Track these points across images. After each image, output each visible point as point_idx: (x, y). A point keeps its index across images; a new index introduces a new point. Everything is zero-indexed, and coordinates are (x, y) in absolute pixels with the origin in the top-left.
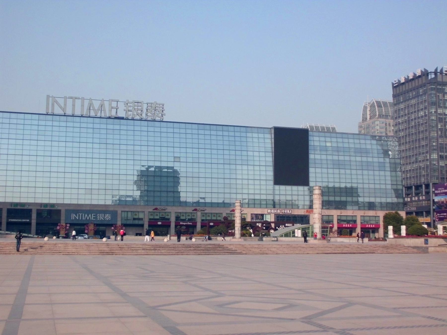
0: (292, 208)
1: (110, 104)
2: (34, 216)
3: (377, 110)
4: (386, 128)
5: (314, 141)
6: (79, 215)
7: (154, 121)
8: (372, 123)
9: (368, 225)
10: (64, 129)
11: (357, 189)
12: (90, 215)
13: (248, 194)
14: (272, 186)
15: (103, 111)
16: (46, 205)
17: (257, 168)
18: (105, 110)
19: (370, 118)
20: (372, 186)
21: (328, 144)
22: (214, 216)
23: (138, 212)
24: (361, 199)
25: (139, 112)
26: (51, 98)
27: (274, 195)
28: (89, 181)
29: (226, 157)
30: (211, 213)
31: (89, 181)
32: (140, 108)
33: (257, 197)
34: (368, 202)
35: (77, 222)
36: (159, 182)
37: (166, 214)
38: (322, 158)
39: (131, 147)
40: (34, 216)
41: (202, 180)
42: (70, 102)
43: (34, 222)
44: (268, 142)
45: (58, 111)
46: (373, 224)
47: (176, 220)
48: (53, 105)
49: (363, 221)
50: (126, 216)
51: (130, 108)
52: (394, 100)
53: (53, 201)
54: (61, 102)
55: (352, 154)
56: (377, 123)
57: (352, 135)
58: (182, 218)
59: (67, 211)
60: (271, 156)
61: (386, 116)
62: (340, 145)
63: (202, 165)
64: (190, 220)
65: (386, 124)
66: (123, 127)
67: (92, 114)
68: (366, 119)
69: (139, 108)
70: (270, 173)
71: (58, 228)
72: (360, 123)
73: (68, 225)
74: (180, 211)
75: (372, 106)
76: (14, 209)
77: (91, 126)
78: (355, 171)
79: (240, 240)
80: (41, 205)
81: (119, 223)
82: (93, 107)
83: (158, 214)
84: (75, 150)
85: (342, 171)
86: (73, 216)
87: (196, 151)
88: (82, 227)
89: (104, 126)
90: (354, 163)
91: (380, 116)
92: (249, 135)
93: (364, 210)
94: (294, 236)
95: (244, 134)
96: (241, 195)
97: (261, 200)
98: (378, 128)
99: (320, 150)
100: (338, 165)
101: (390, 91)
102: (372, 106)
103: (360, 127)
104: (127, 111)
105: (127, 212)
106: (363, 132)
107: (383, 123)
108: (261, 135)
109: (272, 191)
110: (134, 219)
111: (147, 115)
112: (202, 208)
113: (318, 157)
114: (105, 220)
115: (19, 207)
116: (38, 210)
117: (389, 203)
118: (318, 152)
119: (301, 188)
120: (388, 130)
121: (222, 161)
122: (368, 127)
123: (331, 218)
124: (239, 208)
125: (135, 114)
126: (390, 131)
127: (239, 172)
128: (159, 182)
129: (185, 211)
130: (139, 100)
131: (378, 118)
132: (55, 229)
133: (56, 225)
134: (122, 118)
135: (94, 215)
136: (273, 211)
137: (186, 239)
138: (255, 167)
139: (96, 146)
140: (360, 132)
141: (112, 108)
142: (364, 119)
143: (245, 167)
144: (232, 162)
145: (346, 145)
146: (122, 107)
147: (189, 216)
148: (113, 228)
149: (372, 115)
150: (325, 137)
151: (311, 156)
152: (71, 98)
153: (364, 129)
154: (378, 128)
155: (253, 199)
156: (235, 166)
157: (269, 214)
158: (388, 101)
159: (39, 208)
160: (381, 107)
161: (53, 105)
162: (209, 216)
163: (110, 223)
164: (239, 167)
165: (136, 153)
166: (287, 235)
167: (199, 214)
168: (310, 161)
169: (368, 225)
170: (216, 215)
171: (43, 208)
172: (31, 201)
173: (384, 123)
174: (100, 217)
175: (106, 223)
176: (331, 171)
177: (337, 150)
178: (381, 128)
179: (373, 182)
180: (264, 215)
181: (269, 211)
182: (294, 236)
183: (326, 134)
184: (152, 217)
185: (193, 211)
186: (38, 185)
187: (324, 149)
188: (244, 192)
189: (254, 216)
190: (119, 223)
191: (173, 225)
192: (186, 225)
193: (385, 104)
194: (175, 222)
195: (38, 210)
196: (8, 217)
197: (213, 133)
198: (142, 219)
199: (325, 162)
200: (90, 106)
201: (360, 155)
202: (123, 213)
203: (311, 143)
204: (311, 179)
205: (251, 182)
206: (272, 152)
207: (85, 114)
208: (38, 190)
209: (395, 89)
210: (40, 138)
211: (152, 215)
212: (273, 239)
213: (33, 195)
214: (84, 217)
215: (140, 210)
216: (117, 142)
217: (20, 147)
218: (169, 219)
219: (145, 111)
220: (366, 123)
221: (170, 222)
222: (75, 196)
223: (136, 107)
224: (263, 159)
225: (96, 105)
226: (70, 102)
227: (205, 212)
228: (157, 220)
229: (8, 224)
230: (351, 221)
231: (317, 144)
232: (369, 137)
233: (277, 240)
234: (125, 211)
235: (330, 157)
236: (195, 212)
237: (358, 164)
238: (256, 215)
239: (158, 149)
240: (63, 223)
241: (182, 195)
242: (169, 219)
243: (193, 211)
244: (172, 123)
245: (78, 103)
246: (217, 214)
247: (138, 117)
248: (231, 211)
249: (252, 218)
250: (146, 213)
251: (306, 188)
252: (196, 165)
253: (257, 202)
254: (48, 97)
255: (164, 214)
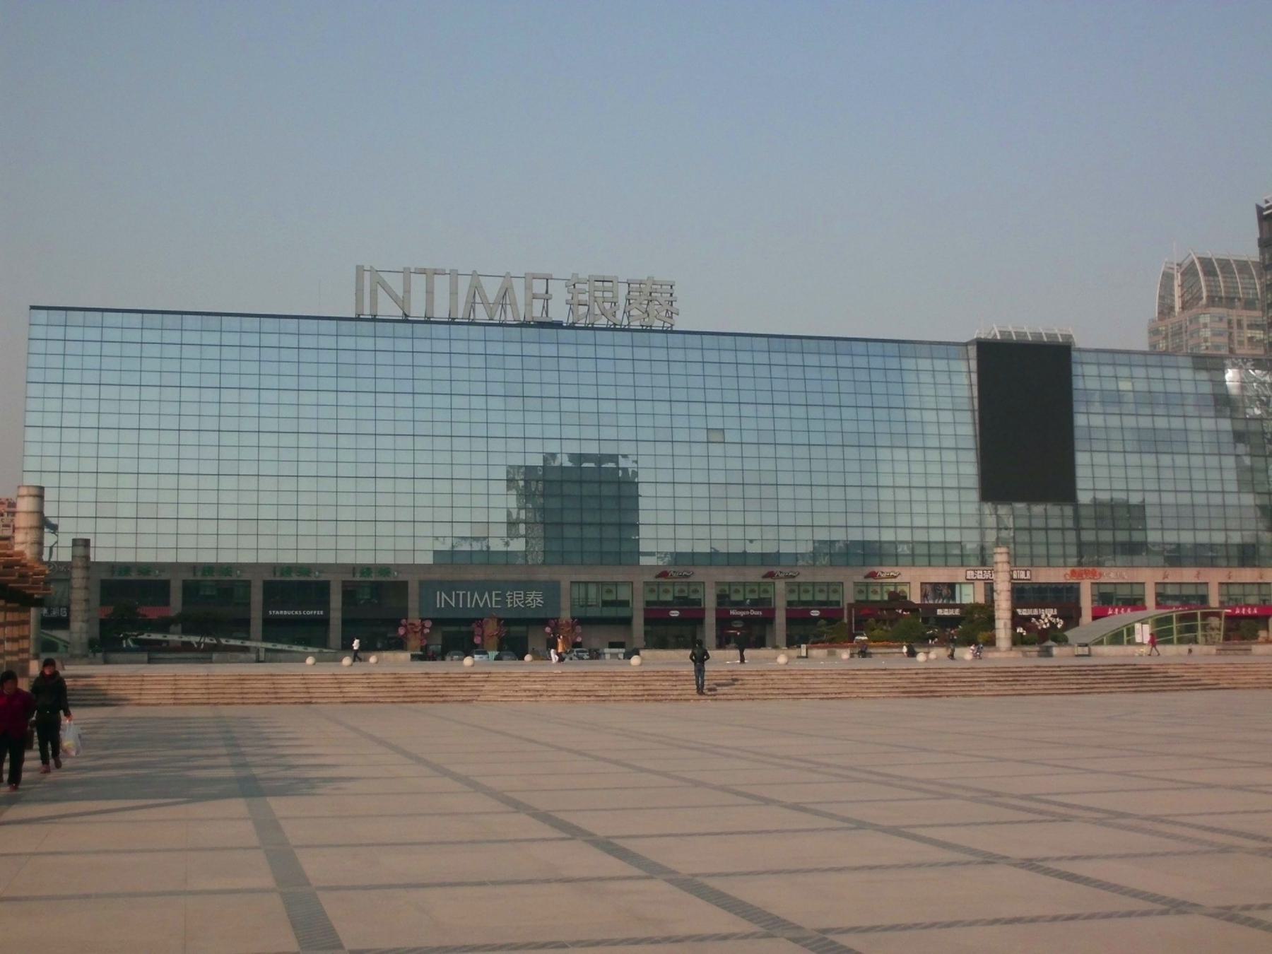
0: (1032, 566)
1: (528, 287)
2: (336, 600)
3: (1203, 284)
4: (1231, 334)
5: (1086, 378)
6: (457, 596)
7: (649, 330)
8: (1191, 322)
9: (1241, 608)
10: (407, 359)
11: (1142, 507)
12: (486, 595)
13: (912, 528)
14: (976, 506)
15: (509, 307)
16: (209, 568)
17: (933, 455)
18: (514, 304)
19: (1183, 308)
20: (1185, 499)
21: (1125, 385)
22: (821, 591)
23: (616, 584)
24: (1153, 537)
25: (607, 305)
26: (367, 275)
27: (1063, 529)
28: (480, 501)
29: (848, 427)
30: (814, 584)
31: (480, 501)
32: (610, 295)
33: (936, 536)
34: (1238, 545)
35: (451, 616)
36: (580, 501)
37: (692, 588)
38: (1109, 424)
39: (589, 406)
40: (336, 600)
41: (785, 492)
42: (419, 282)
43: (336, 616)
44: (962, 381)
45: (388, 308)
46: (1252, 607)
47: (719, 604)
48: (374, 293)
49: (1225, 599)
50: (582, 595)
51: (584, 297)
52: (1262, 253)
53: (385, 559)
54: (396, 283)
55: (1190, 410)
56: (1205, 319)
57: (1142, 357)
58: (736, 597)
59: (422, 584)
60: (970, 420)
61: (1230, 301)
62: (1158, 387)
63: (783, 452)
64: (756, 603)
65: (1229, 322)
66: (567, 351)
67: (481, 314)
68: (1172, 308)
69: (606, 294)
70: (970, 469)
71: (401, 631)
72: (1153, 321)
73: (428, 624)
74: (729, 578)
75: (1189, 272)
76: (301, 582)
77: (478, 347)
78: (1201, 458)
79: (1012, 654)
80: (354, 568)
81: (566, 615)
82: (484, 297)
83: (670, 588)
84: (439, 415)
85: (1166, 460)
86: (441, 599)
87: (766, 411)
88: (463, 629)
89: (514, 348)
90: (1197, 438)
91: (1213, 301)
92: (909, 363)
93: (1228, 566)
94: (1131, 642)
95: (893, 363)
96: (892, 531)
97: (913, 543)
98: (1208, 333)
99: (1103, 402)
100: (1153, 442)
101: (1252, 231)
102: (1189, 272)
103: (1154, 332)
104: (572, 305)
105: (586, 583)
106: (1162, 346)
107: (1221, 319)
108: (940, 365)
109: (977, 518)
110: (605, 603)
111: (627, 312)
112: (787, 571)
113: (1097, 421)
114: (527, 608)
115: (294, 577)
116: (345, 584)
117: (1202, 545)
118: (1097, 407)
119: (1054, 510)
120: (1236, 339)
121: (836, 439)
122: (1178, 332)
123: (1137, 591)
124: (1006, 567)
125: (597, 312)
126: (1241, 343)
127: (885, 467)
128: (580, 501)
129: (741, 579)
130: (607, 274)
131: (1207, 306)
132: (389, 635)
133: (397, 623)
134: (557, 325)
135: (497, 595)
136: (980, 575)
137: (852, 655)
138: (928, 452)
139: (495, 403)
140: (1153, 346)
141: (535, 297)
142: (1166, 310)
143: (900, 454)
144: (867, 440)
145: (1173, 387)
146: (560, 294)
147: (752, 591)
148: (548, 629)
149: (1187, 297)
150: (1162, 367)
151: (1080, 420)
152: (423, 272)
153: (1166, 338)
154: (1208, 333)
155: (825, 542)
156: (872, 450)
157: (970, 582)
158: (1232, 259)
159: (349, 578)
160: (1215, 275)
161: (374, 293)
162: (807, 591)
163: (543, 616)
164: (884, 454)
165: (605, 420)
166: (1116, 639)
167: (780, 585)
168: (1078, 433)
169: (1241, 608)
170: (825, 588)
171: (358, 578)
172: (168, 557)
173: (1225, 320)
174: (515, 600)
175: (530, 615)
176: (1133, 459)
177: (1149, 400)
178: (1214, 335)
179: (1218, 487)
180: (957, 587)
181: (970, 574)
182: (1131, 642)
183: (1149, 357)
184: (653, 598)
185: (765, 577)
186: (346, 514)
187: (1116, 398)
188: (899, 524)
189: (929, 588)
190: (566, 615)
191: (710, 619)
192: (745, 619)
193: (1243, 266)
194: (717, 610)
195: (345, 584)
196: (268, 603)
197: (812, 360)
198: (625, 604)
199: (1116, 435)
200: (476, 289)
201: (1148, 411)
202: (575, 588)
203: (1078, 383)
204: (1080, 484)
205: (918, 495)
206: (973, 411)
207: (460, 314)
208: (344, 529)
209: (1265, 224)
210: (345, 384)
211: (652, 591)
212: (1080, 650)
213: (330, 543)
214: (474, 601)
215: (620, 578)
216: (552, 391)
217: (291, 412)
218: (698, 602)
219: (622, 302)
220: (1168, 321)
221: (703, 610)
222: (211, 542)
223: (597, 294)
224: (948, 430)
225: (492, 289)
226: (419, 282)
227: (797, 580)
228: (669, 605)
229: (268, 622)
230: (1193, 597)
231: (1092, 384)
232: (1188, 362)
233: (1089, 655)
234: (579, 582)
235: (1130, 422)
236: (769, 580)
237: (1206, 438)
238: (935, 586)
239: (663, 408)
240: (414, 616)
241: (644, 532)
242: (698, 602)
243: (765, 577)
244: (698, 337)
245: (442, 284)
246: (828, 584)
247: (602, 322)
248: (866, 577)
249: (924, 596)
250: (639, 586)
251: (1068, 510)
252: (767, 451)
253: (936, 550)
254: (360, 270)
255: (685, 588)
